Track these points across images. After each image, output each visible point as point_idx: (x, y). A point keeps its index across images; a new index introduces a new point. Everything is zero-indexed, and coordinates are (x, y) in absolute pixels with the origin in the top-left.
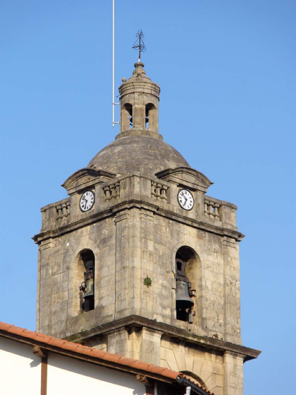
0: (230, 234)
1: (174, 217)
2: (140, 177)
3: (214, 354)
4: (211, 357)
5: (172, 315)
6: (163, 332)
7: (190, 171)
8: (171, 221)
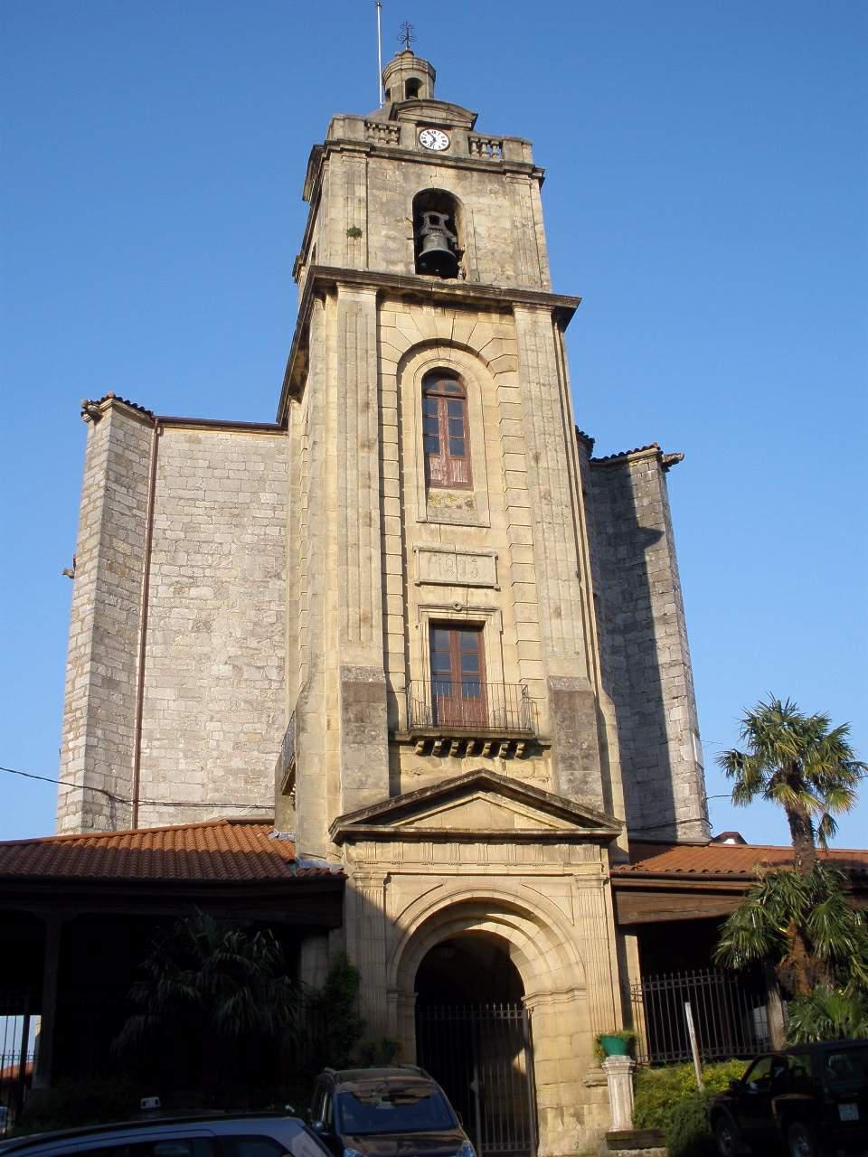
0: (515, 169)
1: (407, 157)
2: (344, 120)
3: (496, 313)
4: (491, 318)
6: (377, 285)
7: (434, 105)
8: (403, 163)
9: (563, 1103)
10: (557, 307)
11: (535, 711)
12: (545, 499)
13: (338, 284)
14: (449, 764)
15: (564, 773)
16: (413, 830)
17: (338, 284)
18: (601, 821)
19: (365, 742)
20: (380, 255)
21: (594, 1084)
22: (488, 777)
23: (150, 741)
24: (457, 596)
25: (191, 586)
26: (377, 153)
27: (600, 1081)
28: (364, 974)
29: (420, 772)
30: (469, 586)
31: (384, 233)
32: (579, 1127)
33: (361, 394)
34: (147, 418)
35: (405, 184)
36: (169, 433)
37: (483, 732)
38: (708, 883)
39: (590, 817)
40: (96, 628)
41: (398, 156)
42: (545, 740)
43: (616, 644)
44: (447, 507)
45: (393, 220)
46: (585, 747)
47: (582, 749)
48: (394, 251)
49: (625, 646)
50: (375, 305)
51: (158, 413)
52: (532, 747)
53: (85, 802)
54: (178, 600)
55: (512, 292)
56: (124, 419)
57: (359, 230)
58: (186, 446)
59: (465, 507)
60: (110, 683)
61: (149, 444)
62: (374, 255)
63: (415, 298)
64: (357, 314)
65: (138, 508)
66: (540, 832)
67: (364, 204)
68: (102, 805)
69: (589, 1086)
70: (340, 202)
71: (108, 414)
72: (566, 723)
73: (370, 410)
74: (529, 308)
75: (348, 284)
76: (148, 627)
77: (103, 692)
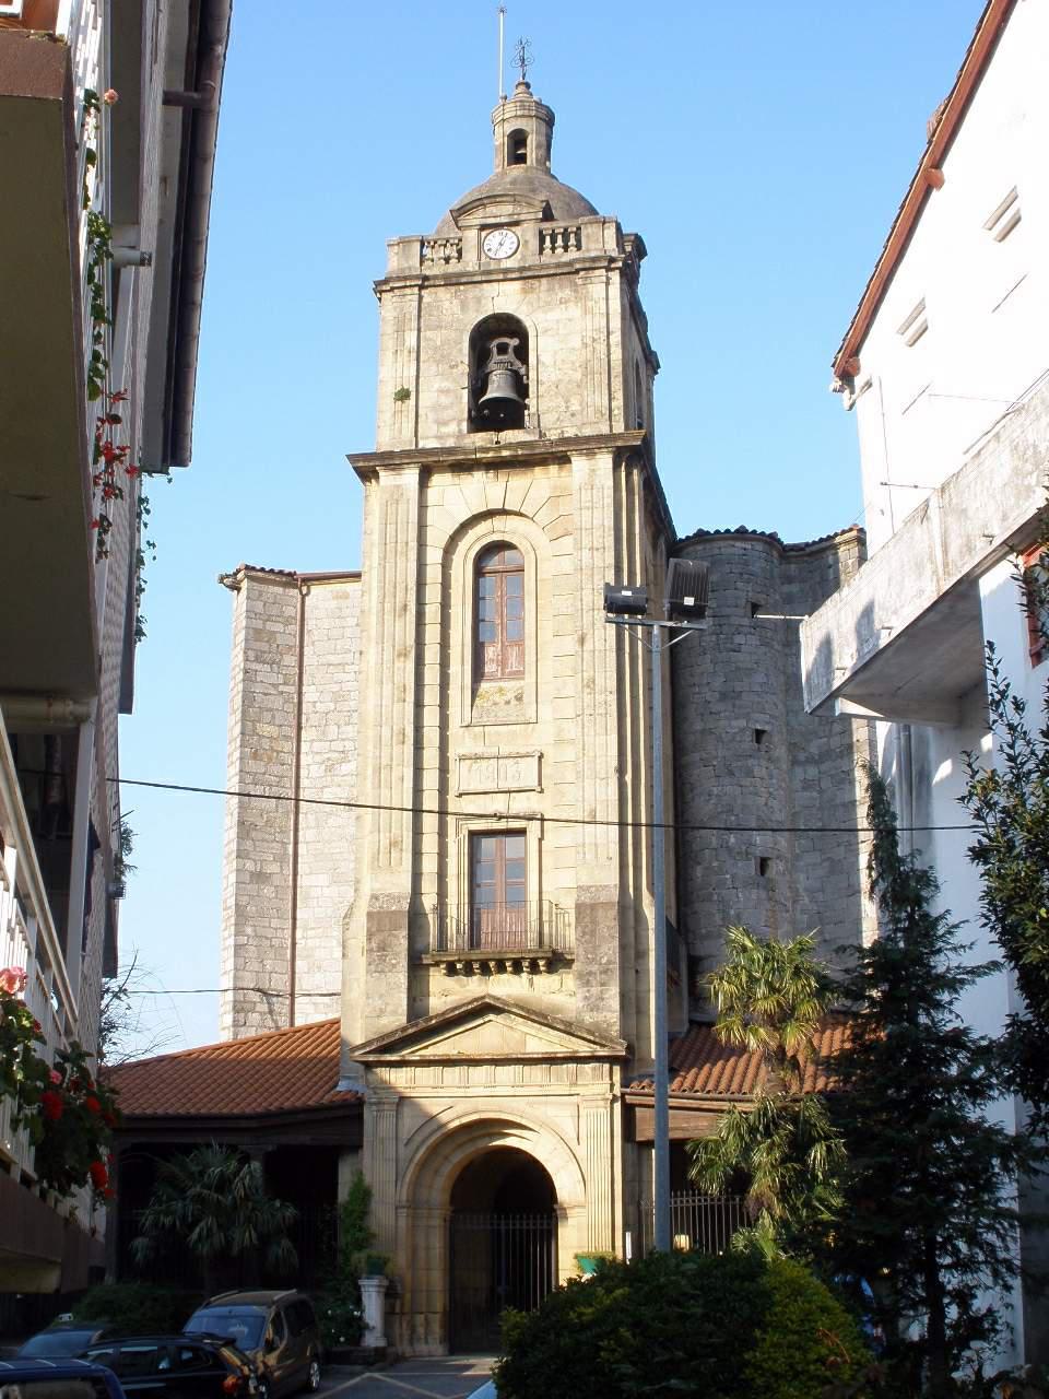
0: (587, 265)
1: (464, 280)
3: (554, 464)
5: (460, 431)
8: (462, 287)
10: (618, 447)
12: (589, 687)
13: (377, 468)
14: (476, 983)
16: (418, 1058)
17: (377, 468)
18: (604, 1042)
19: (387, 970)
20: (431, 416)
22: (492, 1002)
24: (498, 804)
25: (344, 761)
26: (431, 282)
28: (375, 1191)
29: (445, 992)
30: (510, 792)
31: (436, 386)
33: (400, 596)
34: (290, 579)
35: (458, 314)
36: (317, 591)
37: (500, 952)
38: (715, 1103)
40: (241, 823)
41: (454, 280)
44: (495, 704)
45: (446, 367)
47: (601, 964)
48: (446, 408)
50: (417, 486)
51: (302, 569)
52: (557, 961)
53: (235, 1001)
54: (329, 778)
55: (564, 441)
56: (264, 587)
57: (408, 390)
58: (334, 604)
59: (513, 702)
60: (260, 877)
61: (295, 607)
62: (424, 417)
63: (463, 465)
64: (397, 500)
65: (285, 684)
66: (540, 1056)
67: (414, 355)
68: (255, 1003)
70: (389, 355)
71: (244, 585)
72: (587, 937)
73: (408, 613)
74: (587, 455)
75: (387, 467)
77: (252, 888)
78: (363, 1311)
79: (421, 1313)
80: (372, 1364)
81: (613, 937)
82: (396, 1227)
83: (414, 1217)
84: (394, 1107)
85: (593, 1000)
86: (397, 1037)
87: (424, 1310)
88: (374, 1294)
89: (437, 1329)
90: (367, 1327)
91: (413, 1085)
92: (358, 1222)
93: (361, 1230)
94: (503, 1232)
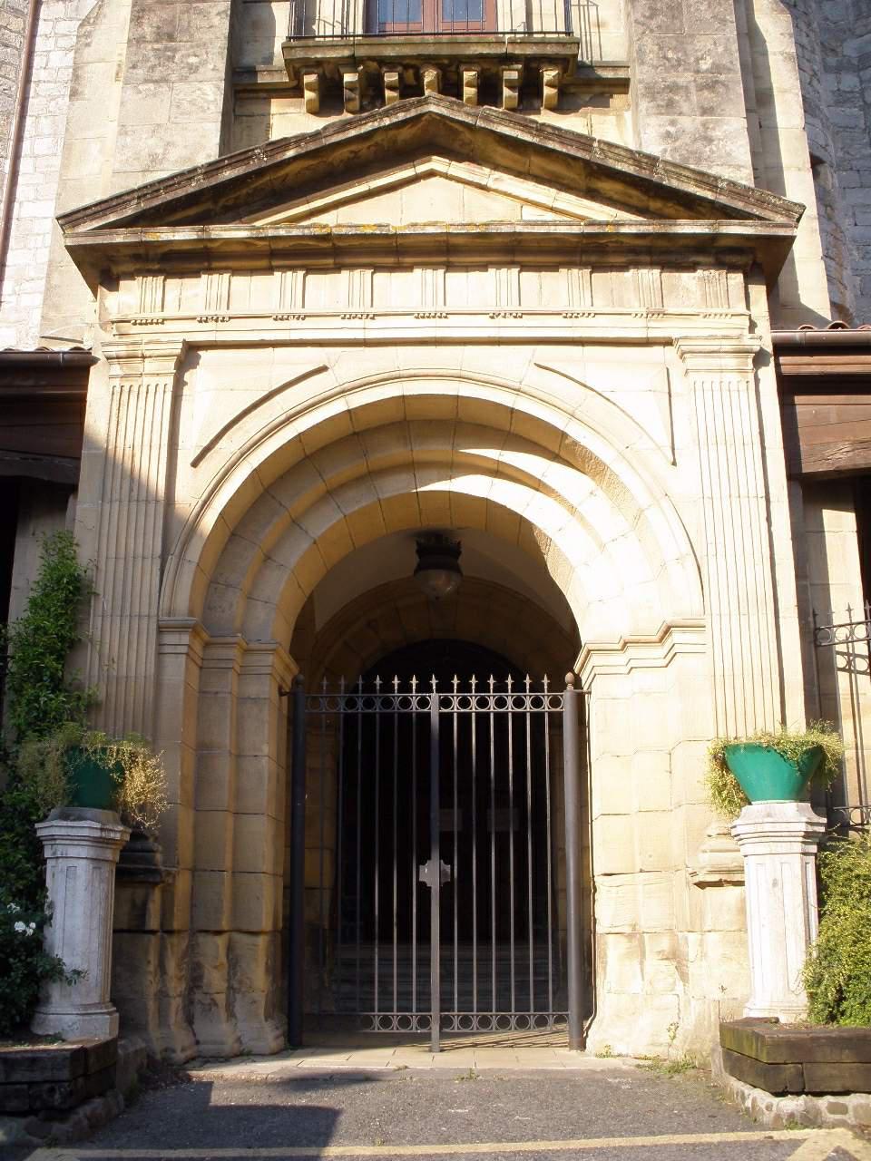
9: (644, 925)
11: (593, 19)
15: (654, 120)
18: (740, 205)
19: (174, 77)
21: (715, 878)
23: (19, 283)
27: (729, 872)
32: (680, 987)
39: (709, 195)
42: (615, 67)
43: (845, 86)
46: (705, 65)
47: (698, 72)
49: (862, 92)
69: (701, 885)
72: (660, 19)
76: (29, 113)
78: (44, 922)
79: (219, 933)
80: (62, 1114)
81: (723, 21)
82: (158, 684)
83: (205, 667)
84: (170, 366)
85: (686, 139)
86: (193, 187)
87: (225, 925)
88: (83, 868)
89: (259, 977)
90: (55, 971)
91: (223, 312)
92: (50, 661)
93: (57, 685)
94: (435, 719)
